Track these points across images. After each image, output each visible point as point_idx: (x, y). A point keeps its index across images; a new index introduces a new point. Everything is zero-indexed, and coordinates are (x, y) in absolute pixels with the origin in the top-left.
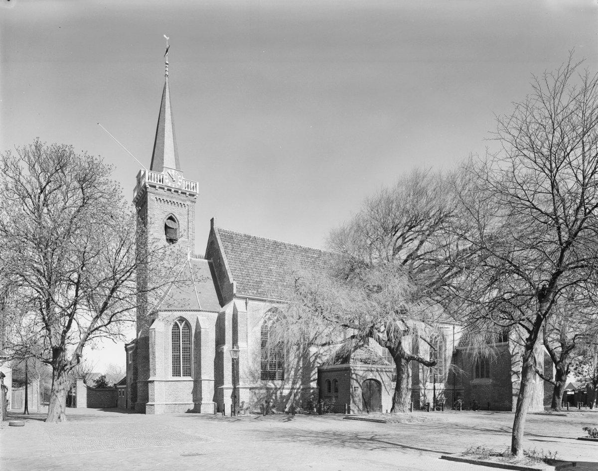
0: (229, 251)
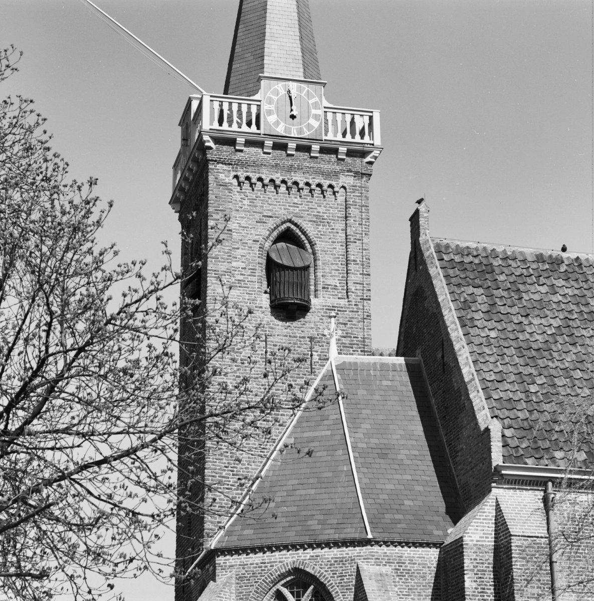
0: (477, 316)
